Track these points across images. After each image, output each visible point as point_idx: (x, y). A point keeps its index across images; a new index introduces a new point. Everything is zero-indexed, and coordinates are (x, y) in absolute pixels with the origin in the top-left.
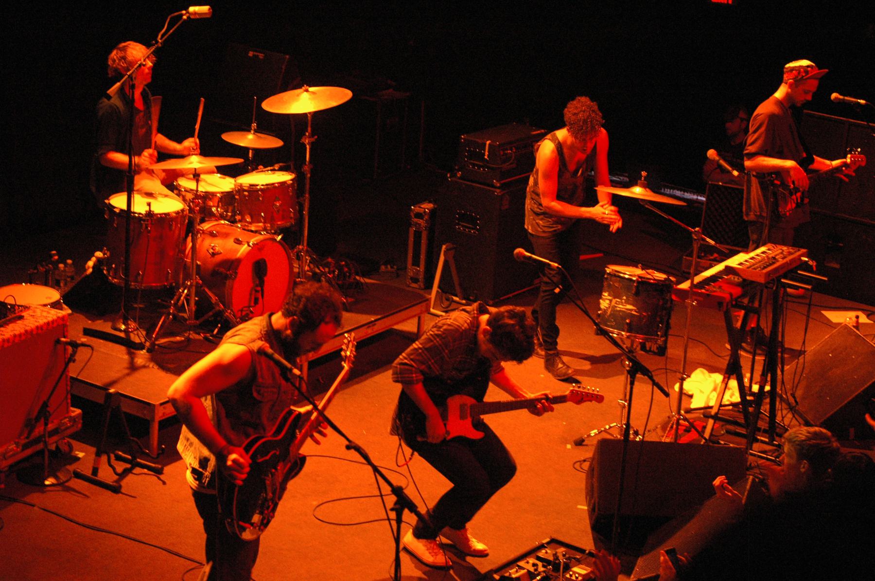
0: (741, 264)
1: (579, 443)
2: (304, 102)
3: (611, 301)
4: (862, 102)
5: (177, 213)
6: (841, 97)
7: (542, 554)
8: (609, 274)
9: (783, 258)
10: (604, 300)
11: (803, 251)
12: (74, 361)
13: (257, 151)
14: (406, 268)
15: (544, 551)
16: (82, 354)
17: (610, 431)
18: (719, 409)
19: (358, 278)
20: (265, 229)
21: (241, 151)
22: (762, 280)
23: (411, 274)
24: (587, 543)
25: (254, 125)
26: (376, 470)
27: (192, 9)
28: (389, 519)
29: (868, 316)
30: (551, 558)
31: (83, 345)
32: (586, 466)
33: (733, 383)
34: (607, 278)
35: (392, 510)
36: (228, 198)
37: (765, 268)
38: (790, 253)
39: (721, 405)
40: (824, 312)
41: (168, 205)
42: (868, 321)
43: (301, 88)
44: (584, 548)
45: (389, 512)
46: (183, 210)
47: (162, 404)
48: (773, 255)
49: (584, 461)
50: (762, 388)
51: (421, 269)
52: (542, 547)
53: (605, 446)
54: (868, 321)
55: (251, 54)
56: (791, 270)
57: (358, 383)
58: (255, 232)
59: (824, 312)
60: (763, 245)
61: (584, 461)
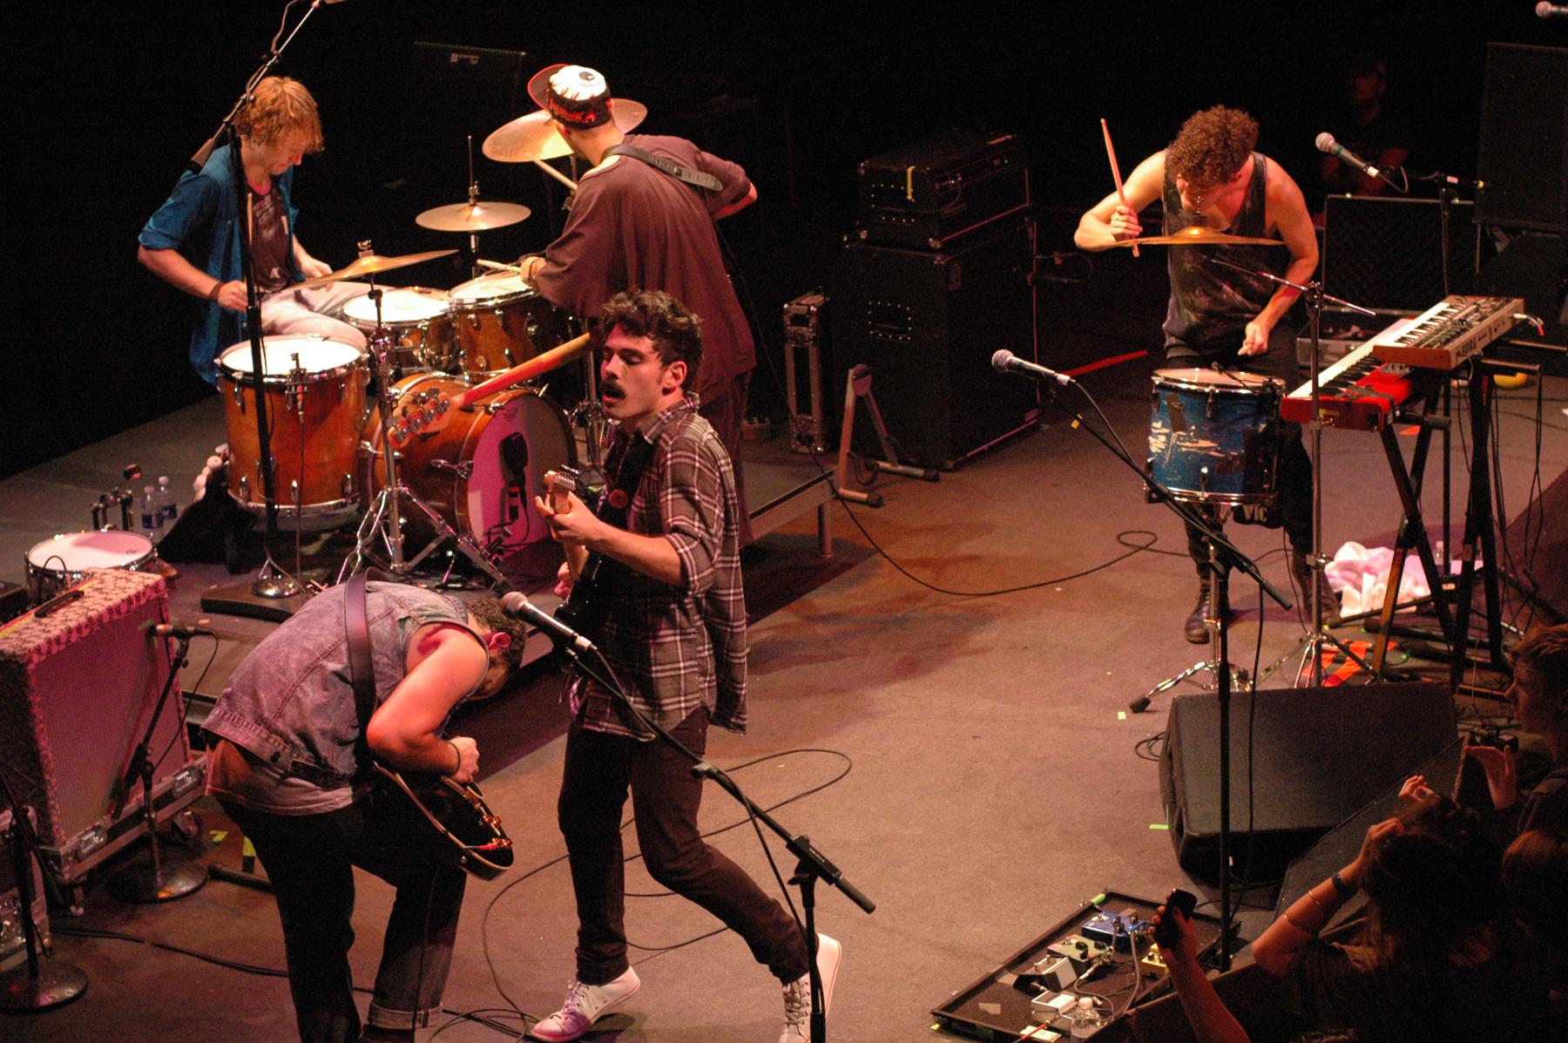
0: (1402, 340)
1: (1140, 706)
3: (1168, 436)
5: (349, 367)
6: (1555, 9)
10: (1156, 436)
13: (480, 234)
16: (199, 650)
17: (1196, 678)
18: (1393, 614)
25: (474, 189)
30: (1110, 932)
33: (1413, 564)
34: (1156, 396)
35: (792, 882)
36: (442, 328)
38: (1495, 310)
46: (358, 361)
48: (1461, 316)
49: (1156, 738)
50: (1467, 566)
51: (816, 415)
52: (1090, 910)
55: (454, 58)
61: (1156, 738)
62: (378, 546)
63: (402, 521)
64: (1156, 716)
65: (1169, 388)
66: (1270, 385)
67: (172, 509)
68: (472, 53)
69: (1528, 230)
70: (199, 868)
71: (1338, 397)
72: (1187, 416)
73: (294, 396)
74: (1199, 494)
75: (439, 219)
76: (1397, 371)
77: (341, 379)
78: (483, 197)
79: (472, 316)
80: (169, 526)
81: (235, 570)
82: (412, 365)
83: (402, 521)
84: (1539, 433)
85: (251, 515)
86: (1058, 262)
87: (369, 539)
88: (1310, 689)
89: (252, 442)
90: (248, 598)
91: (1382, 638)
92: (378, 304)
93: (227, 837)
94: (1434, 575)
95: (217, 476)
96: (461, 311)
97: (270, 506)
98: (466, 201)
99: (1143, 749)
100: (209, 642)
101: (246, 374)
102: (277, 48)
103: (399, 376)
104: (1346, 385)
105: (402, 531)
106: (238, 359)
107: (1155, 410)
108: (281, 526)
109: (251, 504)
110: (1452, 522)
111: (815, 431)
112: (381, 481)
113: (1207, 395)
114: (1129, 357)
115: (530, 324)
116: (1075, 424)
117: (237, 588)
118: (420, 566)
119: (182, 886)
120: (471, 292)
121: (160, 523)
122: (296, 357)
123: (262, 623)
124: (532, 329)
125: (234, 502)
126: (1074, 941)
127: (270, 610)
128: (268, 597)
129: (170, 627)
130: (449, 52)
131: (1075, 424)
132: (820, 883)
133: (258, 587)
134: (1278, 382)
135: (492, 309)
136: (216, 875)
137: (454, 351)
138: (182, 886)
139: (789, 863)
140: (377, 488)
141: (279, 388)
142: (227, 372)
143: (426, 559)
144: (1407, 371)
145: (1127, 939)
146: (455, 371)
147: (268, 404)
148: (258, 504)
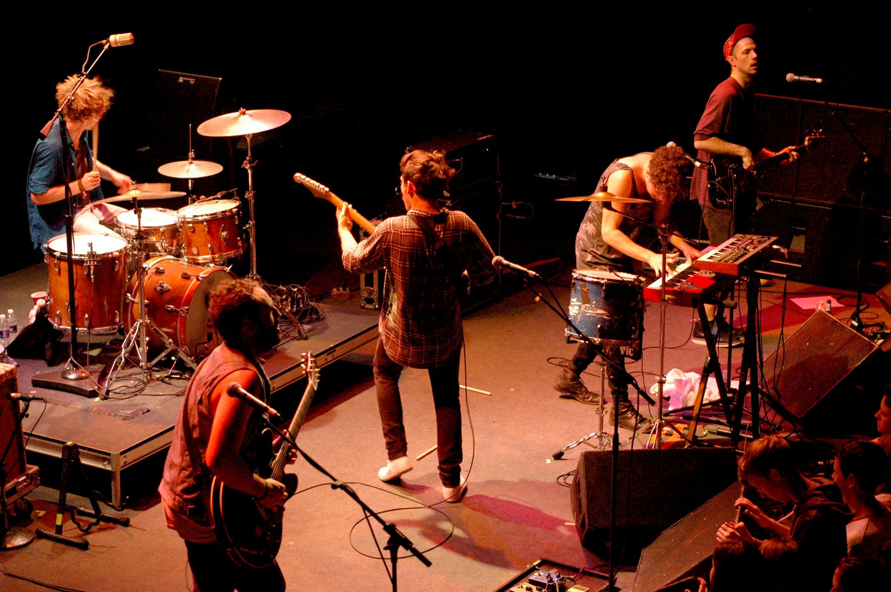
0: (711, 258)
1: (558, 456)
2: (247, 124)
3: (580, 307)
4: (819, 80)
5: (120, 251)
6: (796, 78)
7: (534, 576)
8: (576, 279)
9: (754, 248)
10: (573, 306)
11: (774, 239)
12: (27, 416)
13: (196, 181)
14: (359, 289)
15: (536, 574)
16: (35, 409)
17: (589, 441)
18: (700, 409)
19: (312, 303)
20: (213, 261)
21: (177, 184)
22: (735, 272)
23: (365, 295)
24: (578, 558)
25: (191, 154)
26: (365, 508)
27: (112, 38)
28: (382, 558)
29: (839, 300)
30: (545, 581)
31: (34, 399)
32: (570, 480)
33: (712, 382)
34: (574, 284)
35: (386, 548)
36: (174, 231)
37: (737, 259)
38: (760, 242)
39: (702, 405)
40: (794, 300)
41: (110, 244)
42: (839, 305)
43: (237, 110)
44: (577, 566)
45: (383, 552)
46: (125, 248)
47: (122, 453)
48: (743, 245)
49: (569, 474)
50: (742, 384)
51: (375, 288)
52: (533, 570)
53: (590, 460)
54: (839, 305)
55: (181, 80)
56: (762, 259)
57: (322, 414)
58: (203, 264)
59: (794, 300)
60: (733, 236)
61: (569, 474)
62: (133, 352)
63: (147, 339)
64: (567, 462)
65: (583, 280)
66: (637, 280)
67: (15, 328)
68: (192, 77)
69: (773, 198)
70: (30, 531)
71: (676, 288)
72: (591, 296)
73: (89, 267)
74: (596, 339)
75: (170, 170)
76: (708, 275)
77: (114, 259)
78: (198, 157)
79: (191, 225)
80: (13, 337)
81: (52, 363)
82: (155, 251)
83: (147, 339)
84: (784, 313)
85: (60, 333)
86: (514, 206)
87: (129, 349)
88: (655, 451)
89: (64, 292)
90: (58, 380)
91: (693, 423)
92: (139, 217)
93: (44, 515)
94: (723, 387)
95: (43, 312)
96: (184, 222)
97: (73, 328)
98: (187, 159)
99: (561, 480)
100: (42, 405)
101: (62, 253)
102: (86, 71)
103: (148, 257)
104: (679, 282)
105: (147, 345)
106: (58, 244)
107: (573, 292)
108: (79, 340)
109: (61, 327)
110: (732, 362)
111: (375, 296)
112: (136, 316)
113: (602, 284)
114: (550, 261)
115: (223, 231)
116: (537, 299)
117: (53, 374)
118: (155, 365)
119: (19, 541)
120: (190, 212)
121: (8, 335)
122: (91, 245)
123: (66, 393)
124: (224, 234)
125: (52, 325)
126: (525, 586)
127: (70, 386)
128: (70, 380)
129: (19, 395)
130: (178, 76)
131: (537, 299)
132: (401, 551)
133: (64, 375)
134: (643, 279)
135: (202, 222)
136: (40, 535)
137: (179, 246)
138: (19, 541)
139: (384, 538)
140: (133, 321)
141: (80, 262)
142: (51, 252)
143: (160, 361)
144: (713, 275)
145: (554, 587)
146: (178, 256)
147: (75, 270)
148: (66, 327)
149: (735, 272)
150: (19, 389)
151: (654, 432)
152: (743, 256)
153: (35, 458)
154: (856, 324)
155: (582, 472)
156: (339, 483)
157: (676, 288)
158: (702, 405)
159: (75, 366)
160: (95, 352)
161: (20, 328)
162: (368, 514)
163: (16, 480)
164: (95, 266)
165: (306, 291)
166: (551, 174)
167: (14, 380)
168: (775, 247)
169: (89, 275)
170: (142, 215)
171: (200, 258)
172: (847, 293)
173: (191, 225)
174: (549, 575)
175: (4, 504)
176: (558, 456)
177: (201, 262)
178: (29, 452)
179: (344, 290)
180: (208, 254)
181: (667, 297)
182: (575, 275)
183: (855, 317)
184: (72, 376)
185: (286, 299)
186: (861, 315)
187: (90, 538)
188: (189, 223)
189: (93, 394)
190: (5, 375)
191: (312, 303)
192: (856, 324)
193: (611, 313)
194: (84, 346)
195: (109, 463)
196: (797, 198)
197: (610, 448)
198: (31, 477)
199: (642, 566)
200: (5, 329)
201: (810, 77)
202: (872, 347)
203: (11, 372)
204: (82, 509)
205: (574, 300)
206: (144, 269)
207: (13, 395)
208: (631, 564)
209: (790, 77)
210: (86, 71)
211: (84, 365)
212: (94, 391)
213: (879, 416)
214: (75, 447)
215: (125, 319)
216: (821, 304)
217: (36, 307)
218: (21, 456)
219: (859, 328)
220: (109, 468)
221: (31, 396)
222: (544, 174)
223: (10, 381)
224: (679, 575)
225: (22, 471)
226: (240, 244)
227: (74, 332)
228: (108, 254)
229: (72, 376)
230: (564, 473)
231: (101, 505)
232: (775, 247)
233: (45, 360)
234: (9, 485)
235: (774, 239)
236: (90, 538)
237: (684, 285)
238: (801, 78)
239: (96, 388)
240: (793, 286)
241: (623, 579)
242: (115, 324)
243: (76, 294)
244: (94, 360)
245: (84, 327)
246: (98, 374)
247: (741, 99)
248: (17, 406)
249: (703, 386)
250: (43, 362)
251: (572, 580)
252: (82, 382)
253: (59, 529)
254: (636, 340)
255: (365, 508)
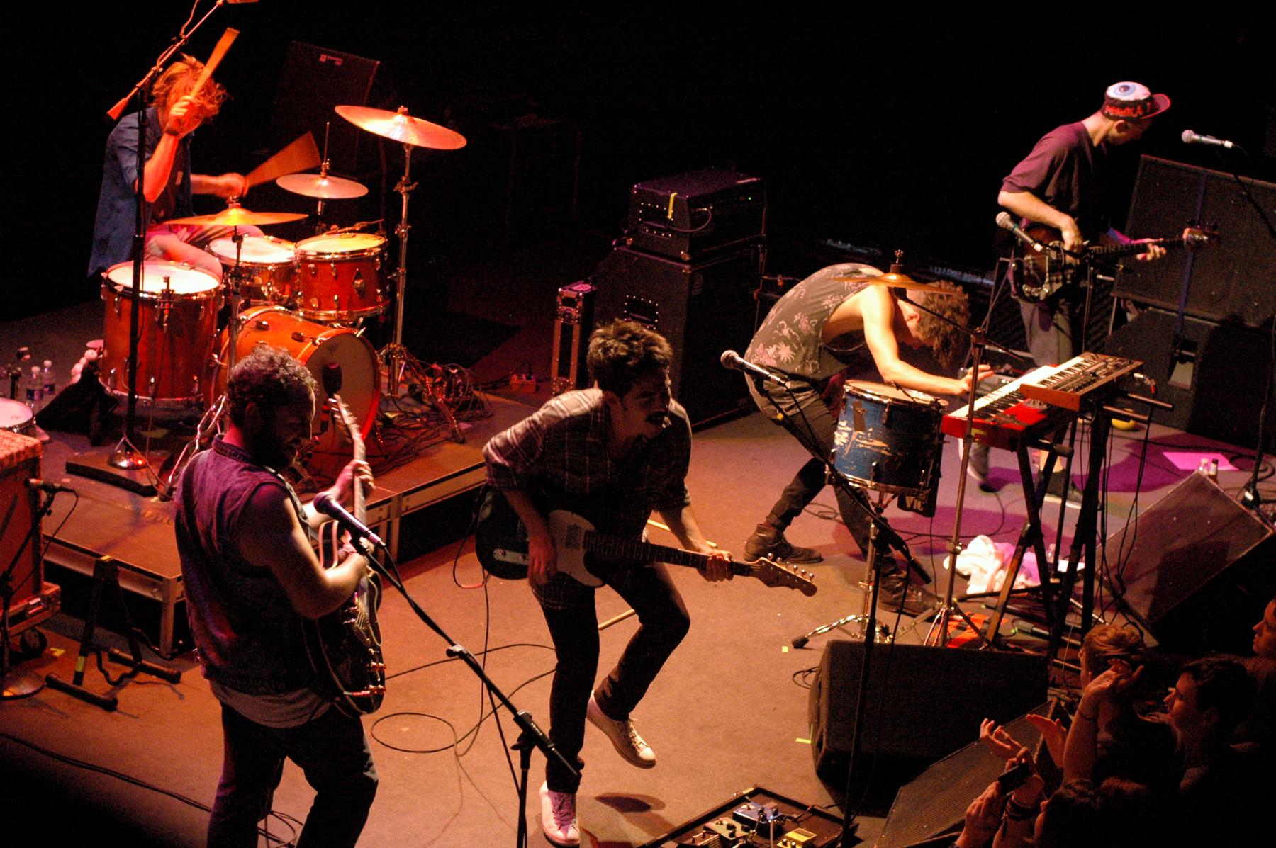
3: (850, 434)
4: (1228, 144)
5: (208, 293)
6: (1197, 137)
7: (741, 811)
8: (849, 394)
13: (328, 202)
14: (549, 379)
16: (62, 503)
17: (847, 627)
19: (477, 393)
20: (339, 319)
22: (1075, 407)
31: (62, 489)
33: (1030, 558)
34: (845, 401)
35: (514, 748)
36: (285, 272)
37: (1080, 388)
39: (1012, 591)
41: (194, 282)
46: (216, 289)
48: (1092, 369)
49: (810, 671)
50: (1072, 566)
52: (741, 800)
53: (837, 650)
55: (323, 58)
56: (1114, 392)
61: (810, 671)
67: (52, 388)
71: (988, 421)
76: (1037, 406)
79: (312, 266)
80: (47, 400)
81: (97, 442)
85: (115, 400)
86: (780, 283)
88: (935, 649)
89: (123, 344)
90: (103, 466)
92: (239, 247)
94: (1045, 569)
97: (132, 394)
101: (125, 288)
102: (186, 33)
103: (247, 306)
104: (995, 412)
106: (122, 275)
109: (116, 392)
119: (25, 688)
121: (41, 397)
122: (167, 280)
126: (725, 823)
128: (121, 468)
129: (41, 482)
139: (514, 733)
141: (151, 303)
142: (111, 284)
144: (1045, 407)
146: (292, 308)
149: (1075, 407)
150: (43, 475)
151: (938, 621)
152: (1089, 384)
153: (55, 573)
154: (1250, 496)
155: (825, 668)
156: (457, 648)
157: (988, 421)
158: (1012, 591)
159: (128, 448)
160: (160, 433)
161: (59, 388)
162: (497, 702)
163: (25, 603)
164: (170, 310)
165: (471, 375)
166: (845, 242)
167: (36, 461)
168: (1137, 375)
169: (161, 322)
170: (243, 246)
171: (322, 313)
172: (1243, 451)
173: (312, 266)
174: (762, 811)
175: (6, 635)
176: (800, 644)
177: (322, 319)
178: (48, 564)
179: (528, 378)
180: (332, 309)
181: (974, 431)
182: (847, 389)
183: (1250, 486)
184: (124, 464)
185: (441, 383)
186: (1259, 485)
187: (121, 695)
188: (311, 262)
189: (150, 492)
190: (24, 452)
191: (477, 393)
192: (1250, 496)
193: (894, 446)
194: (143, 422)
195: (160, 591)
196: (1185, 310)
197: (860, 638)
198: (47, 600)
199: (895, 811)
200: (38, 388)
201: (1218, 138)
202: (1264, 531)
203: (33, 449)
204: (116, 651)
205: (842, 424)
206: (239, 321)
207: (33, 481)
208: (880, 807)
209: (1188, 135)
210: (186, 33)
211: (142, 449)
212: (151, 487)
213: (1260, 629)
214: (114, 563)
215: (204, 389)
216: (1205, 465)
217: (83, 361)
218: (37, 565)
219: (1257, 500)
220: (159, 598)
221: (57, 485)
222: (836, 241)
223: (28, 463)
224: (944, 829)
225: (37, 591)
226: (380, 299)
227: (132, 401)
228: (191, 295)
229: (124, 464)
230: (804, 668)
231: (144, 650)
232: (1137, 375)
233: (89, 437)
234: (13, 609)
235: (1137, 364)
236: (121, 695)
237: (1002, 417)
238: (1204, 139)
239: (155, 482)
240: (1157, 431)
241: (865, 825)
242: (193, 394)
243: (141, 348)
244: (156, 444)
245: (146, 395)
246: (160, 464)
247: (1080, 153)
248: (37, 496)
249: (1016, 562)
250: (85, 438)
251: (795, 820)
252: (138, 473)
253: (79, 677)
254: (925, 488)
255: (491, 687)
